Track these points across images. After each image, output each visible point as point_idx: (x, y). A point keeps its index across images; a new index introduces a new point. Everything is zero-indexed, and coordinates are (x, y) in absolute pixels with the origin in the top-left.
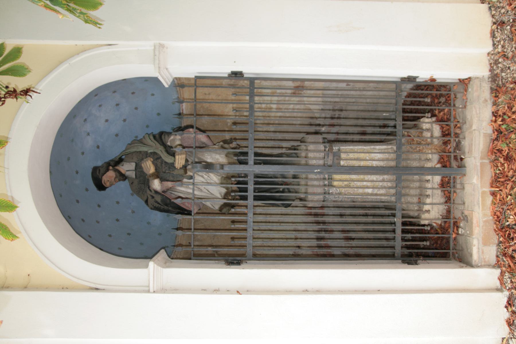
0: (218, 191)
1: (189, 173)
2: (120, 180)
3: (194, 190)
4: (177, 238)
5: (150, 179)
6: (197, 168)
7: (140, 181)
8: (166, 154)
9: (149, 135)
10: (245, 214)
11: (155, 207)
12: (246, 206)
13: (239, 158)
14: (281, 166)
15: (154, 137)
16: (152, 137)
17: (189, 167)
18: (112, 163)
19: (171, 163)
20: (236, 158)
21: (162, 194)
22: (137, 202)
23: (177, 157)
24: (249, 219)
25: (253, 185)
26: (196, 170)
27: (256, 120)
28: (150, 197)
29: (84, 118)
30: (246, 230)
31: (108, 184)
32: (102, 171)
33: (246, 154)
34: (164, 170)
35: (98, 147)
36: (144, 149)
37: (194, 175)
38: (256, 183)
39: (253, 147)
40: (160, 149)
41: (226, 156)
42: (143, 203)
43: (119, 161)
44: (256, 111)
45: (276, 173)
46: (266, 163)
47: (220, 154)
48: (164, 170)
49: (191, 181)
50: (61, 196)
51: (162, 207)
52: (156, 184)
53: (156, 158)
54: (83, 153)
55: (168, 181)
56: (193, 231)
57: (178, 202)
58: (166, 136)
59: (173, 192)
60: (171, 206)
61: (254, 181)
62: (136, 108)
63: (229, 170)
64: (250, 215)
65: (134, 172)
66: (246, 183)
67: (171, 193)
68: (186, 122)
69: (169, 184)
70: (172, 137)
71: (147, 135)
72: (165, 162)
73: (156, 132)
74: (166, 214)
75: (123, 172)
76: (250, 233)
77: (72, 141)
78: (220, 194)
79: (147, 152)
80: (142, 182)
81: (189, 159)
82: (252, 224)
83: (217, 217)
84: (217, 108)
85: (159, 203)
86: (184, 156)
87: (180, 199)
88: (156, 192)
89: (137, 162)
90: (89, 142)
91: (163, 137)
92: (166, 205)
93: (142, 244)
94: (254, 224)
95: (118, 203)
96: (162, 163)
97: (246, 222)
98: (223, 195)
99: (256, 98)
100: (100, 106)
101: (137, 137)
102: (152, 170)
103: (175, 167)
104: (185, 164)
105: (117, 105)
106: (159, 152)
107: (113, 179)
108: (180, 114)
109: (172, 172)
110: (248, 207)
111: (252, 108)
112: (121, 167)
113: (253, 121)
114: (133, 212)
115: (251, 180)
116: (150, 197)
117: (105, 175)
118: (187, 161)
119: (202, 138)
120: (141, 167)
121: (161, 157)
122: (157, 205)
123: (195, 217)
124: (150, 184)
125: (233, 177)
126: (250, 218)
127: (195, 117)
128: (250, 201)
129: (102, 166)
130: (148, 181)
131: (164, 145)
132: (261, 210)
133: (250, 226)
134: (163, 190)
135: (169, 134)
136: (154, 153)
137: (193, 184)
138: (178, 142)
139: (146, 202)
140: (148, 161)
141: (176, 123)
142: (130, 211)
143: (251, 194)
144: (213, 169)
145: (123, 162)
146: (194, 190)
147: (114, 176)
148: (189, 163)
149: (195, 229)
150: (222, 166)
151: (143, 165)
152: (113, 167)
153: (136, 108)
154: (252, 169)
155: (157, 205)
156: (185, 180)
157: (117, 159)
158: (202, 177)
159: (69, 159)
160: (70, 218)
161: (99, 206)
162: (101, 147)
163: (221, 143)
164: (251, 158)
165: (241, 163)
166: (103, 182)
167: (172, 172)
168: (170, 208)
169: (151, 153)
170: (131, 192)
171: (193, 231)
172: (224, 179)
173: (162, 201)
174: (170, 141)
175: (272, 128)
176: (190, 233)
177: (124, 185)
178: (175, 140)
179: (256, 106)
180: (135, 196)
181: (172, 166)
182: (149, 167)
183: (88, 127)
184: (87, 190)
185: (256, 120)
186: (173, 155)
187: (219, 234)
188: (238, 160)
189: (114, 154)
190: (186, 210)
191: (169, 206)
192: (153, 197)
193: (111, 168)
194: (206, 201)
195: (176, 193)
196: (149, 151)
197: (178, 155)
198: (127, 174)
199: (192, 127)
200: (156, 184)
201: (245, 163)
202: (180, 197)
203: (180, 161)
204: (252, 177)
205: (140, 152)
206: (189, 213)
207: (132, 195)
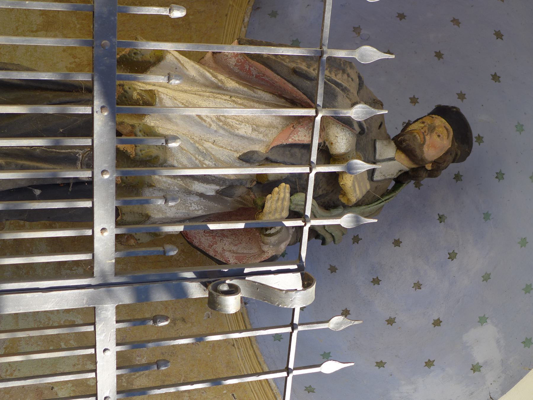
142: (363, 32)
147: (425, 149)
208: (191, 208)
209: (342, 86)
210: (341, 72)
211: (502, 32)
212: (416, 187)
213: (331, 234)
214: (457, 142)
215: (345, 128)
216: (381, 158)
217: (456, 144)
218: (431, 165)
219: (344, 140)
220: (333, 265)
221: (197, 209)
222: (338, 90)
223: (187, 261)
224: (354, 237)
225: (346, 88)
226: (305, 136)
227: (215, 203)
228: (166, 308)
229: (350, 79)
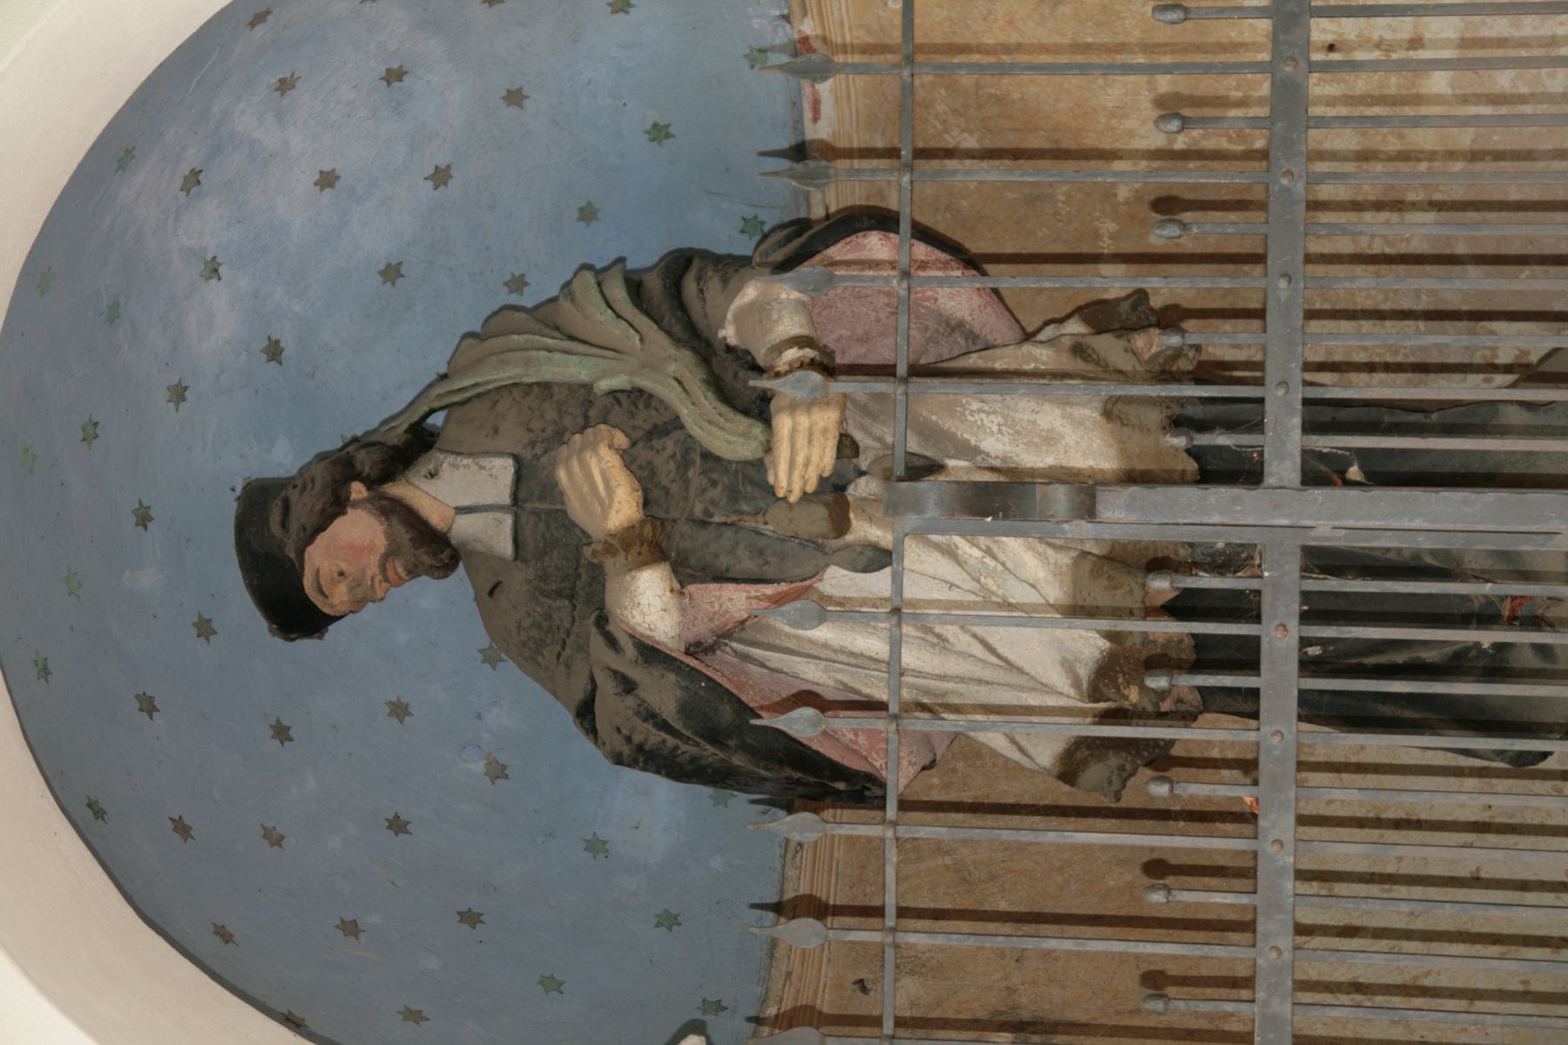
0: (1053, 658)
1: (865, 530)
2: (413, 572)
3: (896, 645)
4: (780, 952)
5: (609, 564)
6: (917, 506)
7: (543, 577)
8: (709, 403)
9: (600, 274)
10: (1245, 818)
11: (640, 748)
12: (1248, 766)
13: (1203, 440)
14: (1491, 496)
15: (635, 287)
16: (618, 293)
17: (863, 488)
18: (366, 461)
19: (746, 463)
20: (1180, 441)
21: (687, 664)
22: (521, 709)
23: (783, 423)
24: (1273, 849)
25: (1293, 624)
26: (912, 520)
27: (1313, 180)
28: (607, 686)
29: (185, 169)
30: (1247, 926)
31: (339, 597)
32: (304, 507)
33: (1249, 417)
34: (698, 510)
35: (274, 351)
36: (572, 368)
37: (899, 542)
38: (1316, 610)
39: (1295, 366)
40: (672, 368)
41: (1108, 414)
42: (565, 718)
43: (412, 446)
44: (1322, 122)
45: (1457, 543)
46: (1388, 474)
47: (1065, 403)
48: (698, 510)
49: (878, 583)
50: (45, 672)
51: (687, 750)
52: (650, 603)
53: (647, 427)
54: (179, 394)
55: (722, 578)
56: (890, 921)
57: (800, 724)
58: (714, 285)
59: (756, 652)
60: (744, 748)
61: (1306, 596)
62: (515, 97)
63: (1127, 517)
64: (1278, 825)
65: (508, 520)
66: (1244, 607)
67: (748, 658)
68: (838, 191)
69: (735, 600)
70: (750, 292)
71: (588, 276)
72: (707, 456)
73: (645, 254)
74: (704, 791)
75: (436, 518)
76: (1273, 948)
77: (114, 314)
78: (1068, 666)
79: (587, 387)
80: (557, 582)
81: (858, 436)
82: (1289, 885)
83: (1051, 837)
84: (1054, 101)
85: (664, 726)
86: (827, 418)
87: (809, 712)
88: (650, 653)
89: (527, 454)
90: (217, 322)
91: (690, 286)
92: (714, 736)
93: (552, 984)
94: (1303, 888)
95: (399, 710)
96: (684, 465)
97: (1249, 873)
98: (1084, 673)
99: (1319, 86)
100: (285, 85)
101: (518, 284)
102: (621, 507)
103: (770, 490)
104: (836, 472)
105: (394, 76)
106: (668, 392)
107: (373, 562)
108: (799, 152)
109: (750, 523)
110: (1265, 767)
111: (1289, 97)
112: (428, 486)
113: (1300, 187)
114: (498, 772)
115: (1281, 587)
116: (607, 686)
117: (322, 539)
118: (847, 447)
119: (959, 297)
120: (551, 490)
121: (676, 424)
122: (655, 737)
123: (903, 832)
124: (610, 599)
125: (1158, 564)
126: (1279, 844)
127: (910, 168)
128: (1279, 731)
129: (300, 481)
130: (597, 578)
131: (697, 339)
132: (1354, 795)
133: (1281, 900)
134: (691, 636)
135: (731, 267)
136: (638, 395)
137: (896, 611)
138: (789, 325)
139: (585, 713)
140: (594, 447)
141: (780, 196)
142: (479, 767)
143: (1279, 679)
144: (1025, 516)
145: (436, 455)
146: (896, 645)
147: (381, 543)
148: (864, 463)
149: (903, 912)
150: (1086, 491)
151: (562, 475)
152: (371, 483)
153: (515, 97)
154: (1284, 517)
155: (655, 737)
156: (838, 580)
157: (397, 436)
158: (951, 553)
159: (91, 432)
160: (99, 814)
161: (282, 733)
162: (289, 344)
163: (1075, 327)
164: (1284, 442)
165: (1217, 471)
166: (308, 583)
167: (750, 523)
168: (738, 760)
169: (613, 393)
170: (485, 641)
171: (890, 921)
172: (1096, 573)
173: (685, 710)
174: (738, 320)
175: (1419, 232)
176: (876, 937)
177: (443, 601)
178: (769, 312)
179: (1319, 86)
180: (510, 669)
181: (751, 478)
182: (603, 487)
183: (208, 227)
184: (205, 629)
185: (1313, 180)
186: (760, 409)
187: (1068, 945)
188: (1194, 453)
189: (376, 397)
190: (839, 771)
191: (731, 743)
192: (628, 686)
193: (358, 490)
194: (983, 727)
195: (775, 659)
196: (604, 385)
197: (793, 407)
198: (465, 529)
199: (884, 221)
200: (650, 603)
201: (1245, 472)
202: (807, 698)
203: (801, 447)
204: (1293, 565)
205: (546, 387)
206: (858, 790)
207: (490, 658)
208: (1001, 420)
209: (656, 725)
210: (647, 748)
211: (466, 927)
212: (277, 342)
213: (619, 316)
214: (290, 560)
215: (648, 633)
216: (499, 515)
217: (292, 555)
218: (353, 496)
219: (644, 601)
220: (514, 110)
221: (983, 416)
222: (677, 725)
223: (940, 127)
224: (445, 184)
225: (645, 720)
226: (731, 599)
227: (936, 424)
228: (1010, 23)
229: (625, 732)
